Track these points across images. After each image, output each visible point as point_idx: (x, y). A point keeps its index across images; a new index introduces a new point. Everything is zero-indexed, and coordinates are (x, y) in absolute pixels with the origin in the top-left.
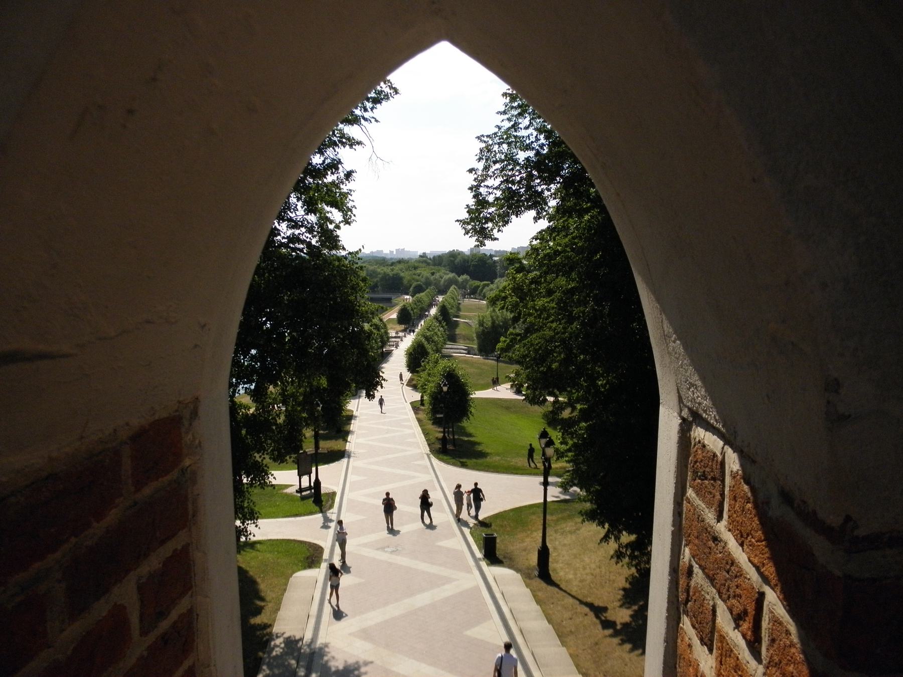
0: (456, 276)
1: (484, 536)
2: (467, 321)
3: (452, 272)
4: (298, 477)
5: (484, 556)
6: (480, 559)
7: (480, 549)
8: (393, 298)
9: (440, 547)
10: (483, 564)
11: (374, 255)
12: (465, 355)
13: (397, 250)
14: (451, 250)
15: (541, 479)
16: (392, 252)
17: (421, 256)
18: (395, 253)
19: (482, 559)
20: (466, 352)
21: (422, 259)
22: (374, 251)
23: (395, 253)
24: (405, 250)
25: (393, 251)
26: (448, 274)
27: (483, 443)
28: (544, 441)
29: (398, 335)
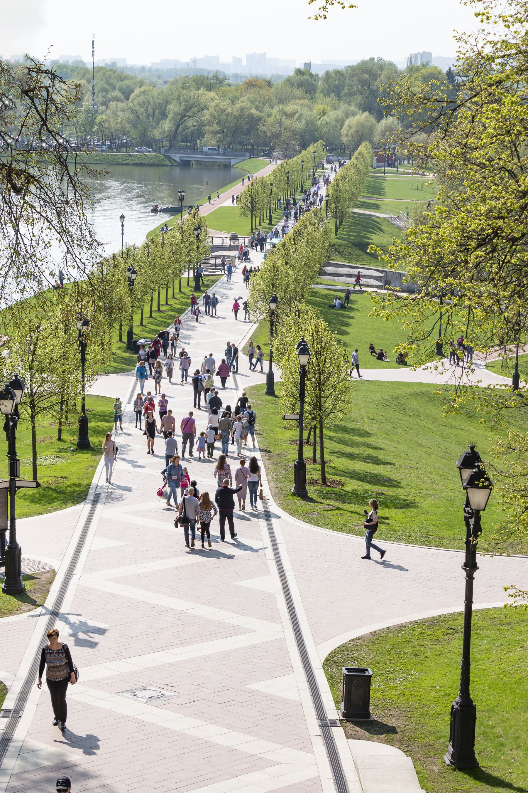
0: (373, 120)
1: (345, 672)
2: (388, 216)
3: (364, 111)
4: (464, 574)
5: (344, 715)
6: (333, 723)
7: (337, 702)
8: (233, 162)
9: (254, 693)
10: (338, 733)
11: (200, 66)
12: (375, 290)
13: (251, 57)
14: (367, 58)
15: (461, 557)
16: (237, 60)
17: (299, 72)
18: (244, 63)
19: (338, 722)
20: (379, 283)
21: (299, 77)
22: (198, 57)
23: (244, 63)
24: (268, 56)
25: (240, 60)
26: (354, 114)
27: (73, 451)
28: (467, 473)
29: (237, 244)
